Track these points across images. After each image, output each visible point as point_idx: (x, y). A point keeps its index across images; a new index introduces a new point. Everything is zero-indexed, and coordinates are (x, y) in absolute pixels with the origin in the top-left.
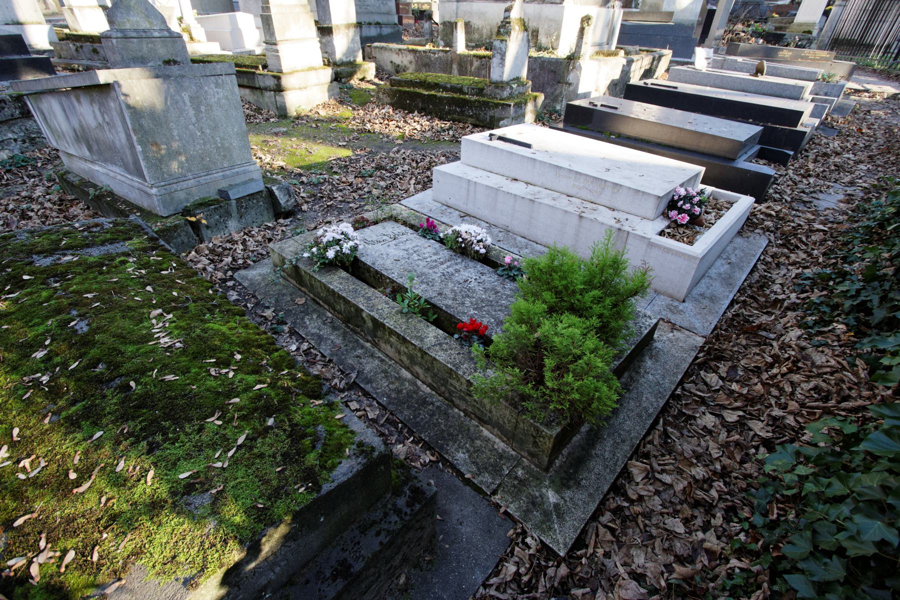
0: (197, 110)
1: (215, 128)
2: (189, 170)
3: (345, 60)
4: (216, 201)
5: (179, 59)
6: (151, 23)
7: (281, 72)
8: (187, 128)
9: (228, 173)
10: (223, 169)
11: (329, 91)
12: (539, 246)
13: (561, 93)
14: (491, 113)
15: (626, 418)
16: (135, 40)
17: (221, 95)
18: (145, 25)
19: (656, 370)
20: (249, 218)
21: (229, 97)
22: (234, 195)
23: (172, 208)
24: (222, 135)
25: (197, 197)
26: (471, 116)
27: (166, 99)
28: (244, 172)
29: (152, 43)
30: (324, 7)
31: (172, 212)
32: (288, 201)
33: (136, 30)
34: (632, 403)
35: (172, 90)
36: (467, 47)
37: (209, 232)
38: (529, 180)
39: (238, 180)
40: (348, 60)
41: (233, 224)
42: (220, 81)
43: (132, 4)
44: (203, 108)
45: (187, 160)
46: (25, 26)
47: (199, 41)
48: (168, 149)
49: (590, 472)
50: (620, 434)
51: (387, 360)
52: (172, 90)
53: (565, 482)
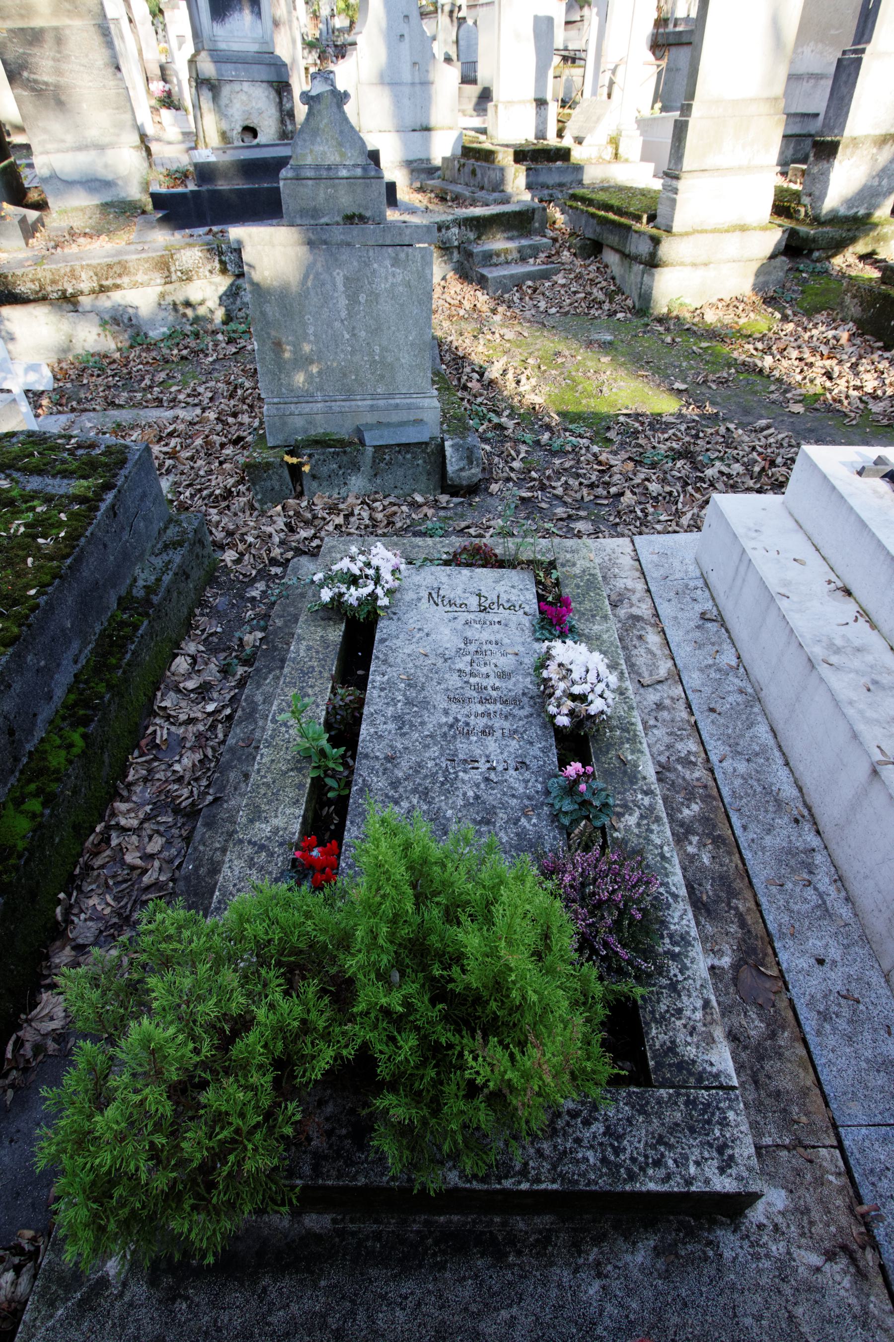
0: (353, 299)
1: (376, 331)
2: (322, 389)
3: (843, 211)
4: (341, 443)
5: (368, 214)
6: (343, 155)
7: (669, 230)
8: (330, 325)
9: (381, 403)
10: (374, 396)
11: (758, 274)
12: (783, 773)
15: (410, 1303)
16: (310, 182)
17: (399, 278)
18: (333, 158)
19: (630, 1292)
20: (389, 479)
21: (413, 283)
22: (372, 439)
23: (281, 437)
24: (385, 343)
25: (319, 430)
27: (306, 277)
28: (409, 407)
29: (333, 186)
30: (842, 99)
31: (279, 443)
32: (462, 469)
33: (318, 167)
34: (467, 1290)
35: (319, 265)
37: (315, 484)
39: (395, 418)
40: (852, 212)
41: (357, 483)
42: (402, 256)
43: (321, 126)
44: (362, 298)
45: (320, 373)
46: (433, 133)
47: (626, 161)
48: (295, 352)
49: (213, 1304)
50: (353, 1313)
52: (319, 265)
53: (163, 1266)
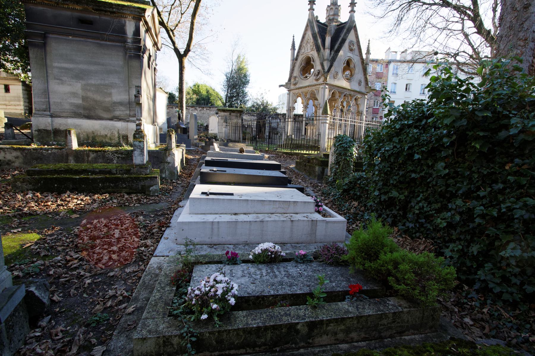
13: (164, 168)
14: (143, 183)
26: (125, 188)
36: (79, 145)
38: (245, 212)
51: (324, 348)
